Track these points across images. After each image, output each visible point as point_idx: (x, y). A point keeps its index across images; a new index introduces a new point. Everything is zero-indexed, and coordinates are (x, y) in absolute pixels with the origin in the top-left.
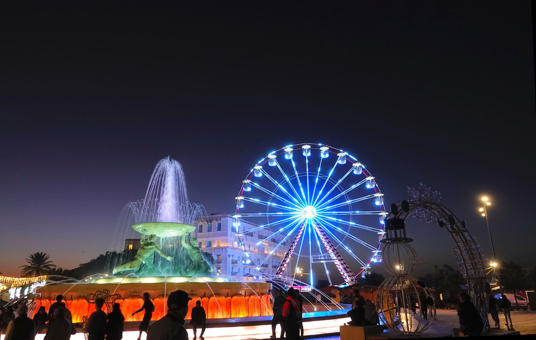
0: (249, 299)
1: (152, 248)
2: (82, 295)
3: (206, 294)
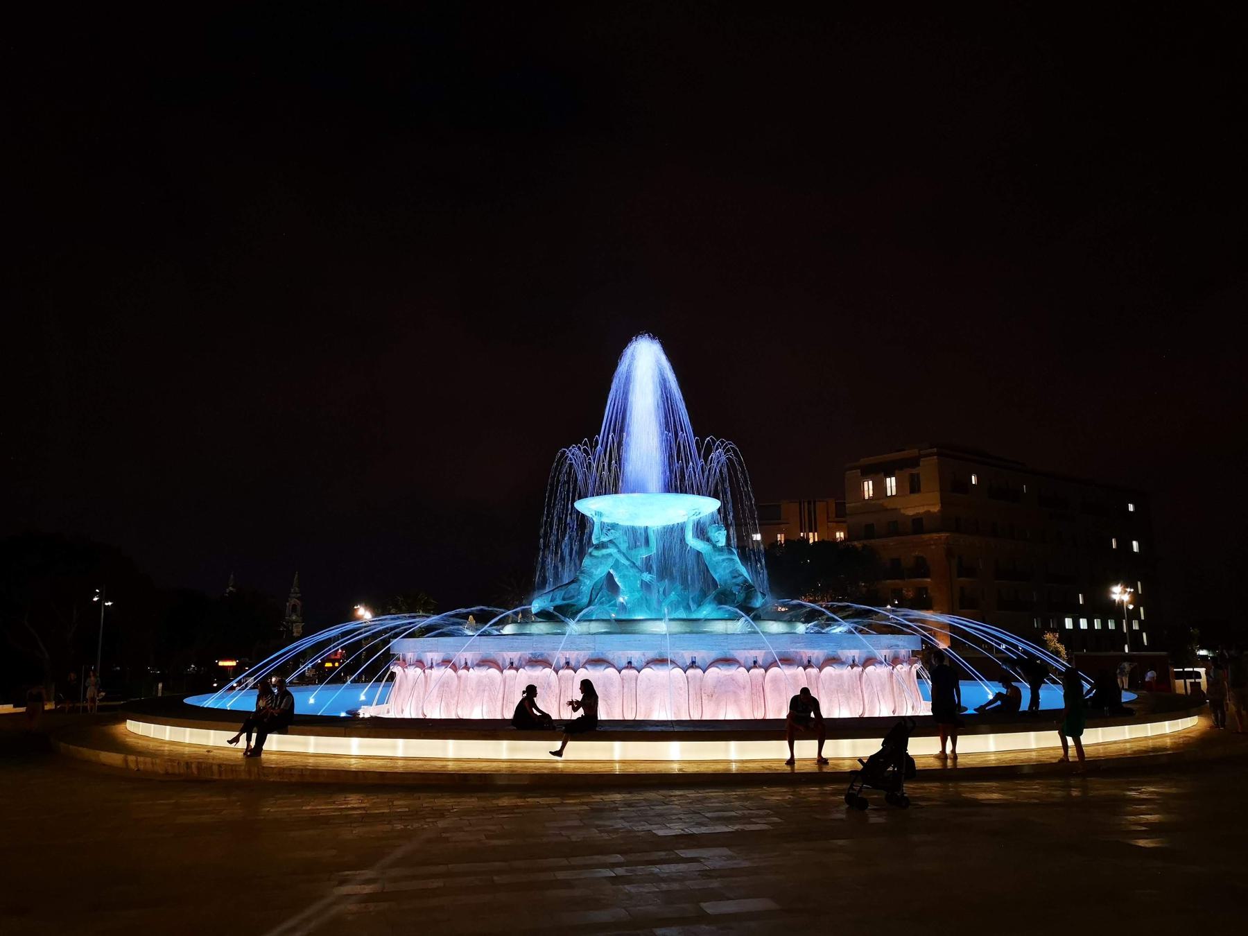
0: (818, 677)
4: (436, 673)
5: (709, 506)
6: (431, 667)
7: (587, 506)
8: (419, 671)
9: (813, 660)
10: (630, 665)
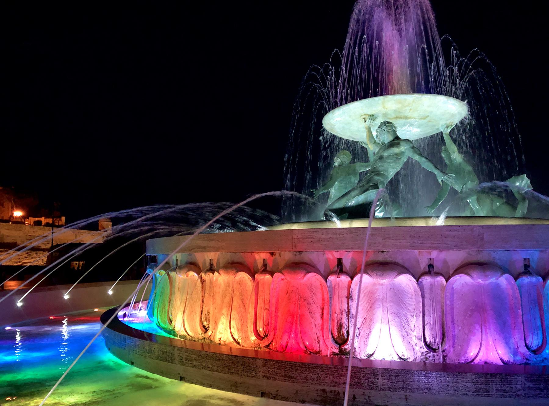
3: (215, 264)
5: (445, 111)
6: (174, 270)
7: (346, 121)
8: (193, 274)
9: (533, 265)
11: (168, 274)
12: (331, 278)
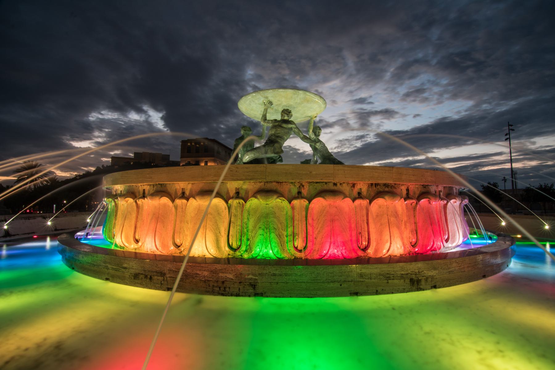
1: (505, 130)
2: (269, 186)
4: (148, 203)
6: (144, 197)
8: (131, 200)
10: (237, 195)
11: (136, 202)
12: (230, 201)
